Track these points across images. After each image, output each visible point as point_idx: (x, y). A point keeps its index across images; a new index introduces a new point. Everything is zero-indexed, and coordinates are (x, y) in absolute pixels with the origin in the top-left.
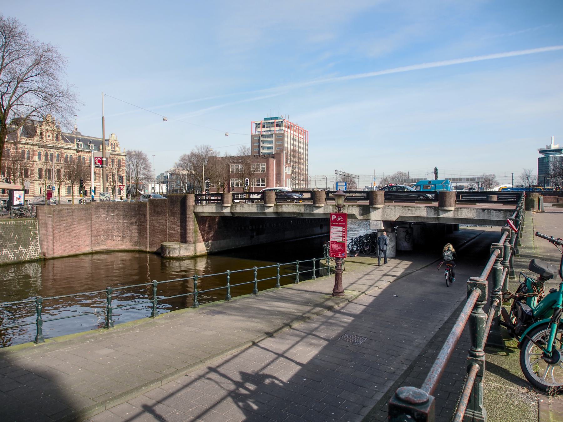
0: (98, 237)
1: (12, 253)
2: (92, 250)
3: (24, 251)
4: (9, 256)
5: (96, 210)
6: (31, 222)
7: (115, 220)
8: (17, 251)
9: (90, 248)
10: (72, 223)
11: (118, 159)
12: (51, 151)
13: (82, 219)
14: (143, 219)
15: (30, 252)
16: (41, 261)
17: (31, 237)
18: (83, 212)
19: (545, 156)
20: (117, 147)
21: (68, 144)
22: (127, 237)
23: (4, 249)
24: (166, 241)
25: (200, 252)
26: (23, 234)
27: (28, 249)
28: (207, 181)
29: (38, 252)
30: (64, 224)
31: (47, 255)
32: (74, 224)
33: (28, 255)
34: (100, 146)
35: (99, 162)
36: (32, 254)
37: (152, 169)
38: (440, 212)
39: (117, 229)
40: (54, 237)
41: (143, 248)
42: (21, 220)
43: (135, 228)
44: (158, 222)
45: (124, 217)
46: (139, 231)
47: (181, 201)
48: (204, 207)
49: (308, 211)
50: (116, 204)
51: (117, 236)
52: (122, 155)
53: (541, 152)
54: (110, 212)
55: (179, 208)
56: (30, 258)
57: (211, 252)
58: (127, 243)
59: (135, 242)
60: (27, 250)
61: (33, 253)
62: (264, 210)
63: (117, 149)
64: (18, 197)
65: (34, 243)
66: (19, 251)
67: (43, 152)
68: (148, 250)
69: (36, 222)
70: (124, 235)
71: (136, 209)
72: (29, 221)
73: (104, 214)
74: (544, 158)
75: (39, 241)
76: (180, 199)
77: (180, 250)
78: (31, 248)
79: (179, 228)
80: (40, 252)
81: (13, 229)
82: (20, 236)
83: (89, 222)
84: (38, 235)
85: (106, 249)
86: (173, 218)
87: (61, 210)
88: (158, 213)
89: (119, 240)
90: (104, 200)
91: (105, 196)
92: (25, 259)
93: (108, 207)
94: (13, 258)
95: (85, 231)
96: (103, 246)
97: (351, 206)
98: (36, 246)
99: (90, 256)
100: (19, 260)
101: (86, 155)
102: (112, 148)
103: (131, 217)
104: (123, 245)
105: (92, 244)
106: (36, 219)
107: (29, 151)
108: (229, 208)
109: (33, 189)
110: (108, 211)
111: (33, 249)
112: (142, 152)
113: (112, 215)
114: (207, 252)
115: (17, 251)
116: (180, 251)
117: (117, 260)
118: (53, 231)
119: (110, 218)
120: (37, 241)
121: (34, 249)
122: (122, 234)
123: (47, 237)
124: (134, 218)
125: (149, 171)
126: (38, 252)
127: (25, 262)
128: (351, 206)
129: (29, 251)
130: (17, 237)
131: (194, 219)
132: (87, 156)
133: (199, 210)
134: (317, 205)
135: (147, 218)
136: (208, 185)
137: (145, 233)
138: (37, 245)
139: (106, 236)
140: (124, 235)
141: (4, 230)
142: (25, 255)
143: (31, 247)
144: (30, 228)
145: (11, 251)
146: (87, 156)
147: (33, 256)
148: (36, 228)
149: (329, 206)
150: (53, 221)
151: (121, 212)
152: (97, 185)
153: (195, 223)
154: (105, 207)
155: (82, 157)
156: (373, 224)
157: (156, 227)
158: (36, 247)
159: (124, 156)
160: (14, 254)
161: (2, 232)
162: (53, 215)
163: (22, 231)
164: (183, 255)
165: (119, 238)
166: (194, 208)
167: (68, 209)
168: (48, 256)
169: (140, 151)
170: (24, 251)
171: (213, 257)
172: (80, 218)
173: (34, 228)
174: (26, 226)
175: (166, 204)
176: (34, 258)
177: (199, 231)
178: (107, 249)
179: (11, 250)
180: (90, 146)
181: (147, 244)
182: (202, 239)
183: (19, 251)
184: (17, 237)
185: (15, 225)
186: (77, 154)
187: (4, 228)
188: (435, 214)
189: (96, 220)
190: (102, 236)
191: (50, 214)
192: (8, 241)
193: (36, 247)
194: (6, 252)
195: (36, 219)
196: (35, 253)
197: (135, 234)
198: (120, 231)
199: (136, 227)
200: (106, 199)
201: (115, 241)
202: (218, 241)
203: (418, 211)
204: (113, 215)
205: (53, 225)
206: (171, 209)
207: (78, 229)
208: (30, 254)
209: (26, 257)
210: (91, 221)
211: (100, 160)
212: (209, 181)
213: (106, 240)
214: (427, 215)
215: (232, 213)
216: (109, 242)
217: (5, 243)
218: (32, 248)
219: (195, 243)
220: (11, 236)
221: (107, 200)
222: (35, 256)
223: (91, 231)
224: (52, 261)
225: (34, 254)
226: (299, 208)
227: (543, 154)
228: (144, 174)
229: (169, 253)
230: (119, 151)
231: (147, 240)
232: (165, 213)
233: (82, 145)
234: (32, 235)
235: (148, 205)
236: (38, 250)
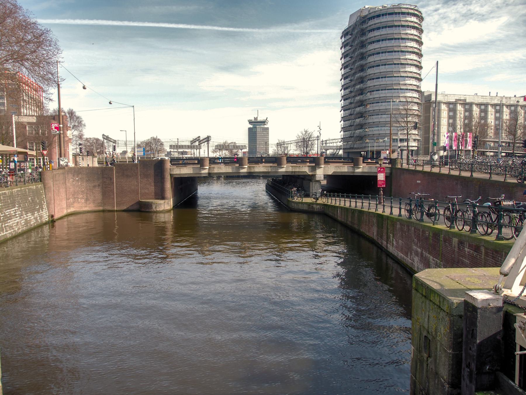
7: (79, 184)
19: (253, 126)
39: (81, 192)
41: (109, 208)
45: (87, 181)
46: (103, 192)
49: (274, 170)
50: (79, 169)
51: (82, 198)
53: (250, 122)
59: (99, 203)
62: (240, 171)
68: (115, 209)
89: (83, 202)
91: (65, 161)
103: (94, 181)
108: (208, 169)
110: (74, 176)
113: (77, 179)
122: (85, 196)
135: (114, 180)
140: (87, 197)
165: (83, 201)
166: (171, 170)
178: (75, 211)
198: (84, 193)
200: (65, 164)
211: (57, 126)
213: (74, 202)
226: (267, 168)
227: (252, 125)
229: (156, 208)
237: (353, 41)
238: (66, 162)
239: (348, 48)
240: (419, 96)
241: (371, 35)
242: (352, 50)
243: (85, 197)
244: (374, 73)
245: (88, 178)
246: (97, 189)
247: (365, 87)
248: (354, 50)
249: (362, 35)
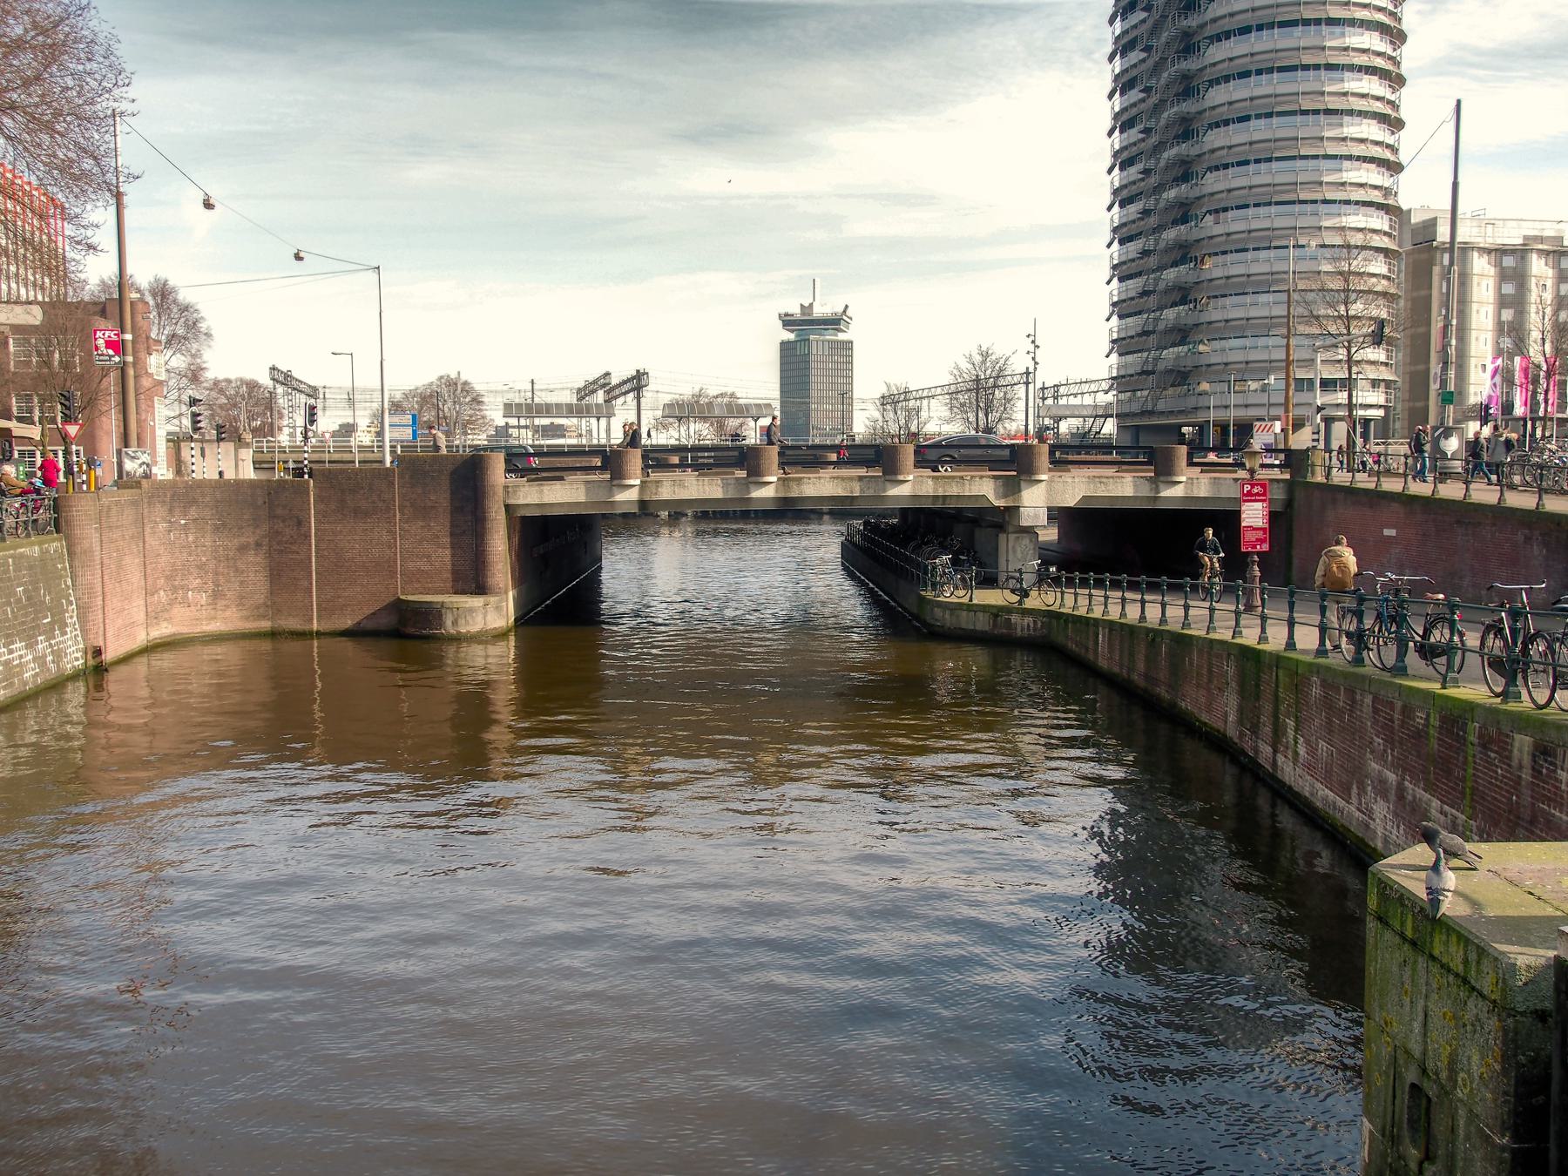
19: (797, 336)
22: (229, 594)
38: (1162, 486)
41: (293, 624)
44: (357, 538)
45: (217, 529)
49: (870, 493)
50: (191, 487)
51: (199, 590)
53: (788, 322)
54: (177, 511)
55: (448, 495)
58: (228, 613)
59: (258, 608)
68: (315, 627)
71: (260, 502)
74: (796, 342)
79: (448, 552)
93: (173, 496)
97: (977, 479)
99: (144, 659)
103: (241, 528)
105: (153, 617)
110: (171, 511)
113: (183, 522)
117: (197, 671)
124: (251, 529)
128: (977, 479)
134: (901, 478)
135: (310, 528)
140: (218, 586)
149: (925, 480)
151: (208, 513)
156: (1028, 516)
164: (492, 627)
165: (204, 598)
178: (174, 634)
188: (1151, 490)
197: (257, 582)
198: (206, 572)
201: (193, 608)
203: (1119, 485)
204: (185, 524)
211: (115, 338)
214: (1136, 492)
226: (848, 484)
227: (792, 331)
229: (455, 623)
231: (311, 597)
237: (1156, 29)
239: (1135, 56)
240: (1391, 227)
241: (1215, 139)
242: (1150, 63)
244: (1228, 187)
247: (1198, 195)
248: (1157, 63)
249: (1184, 8)
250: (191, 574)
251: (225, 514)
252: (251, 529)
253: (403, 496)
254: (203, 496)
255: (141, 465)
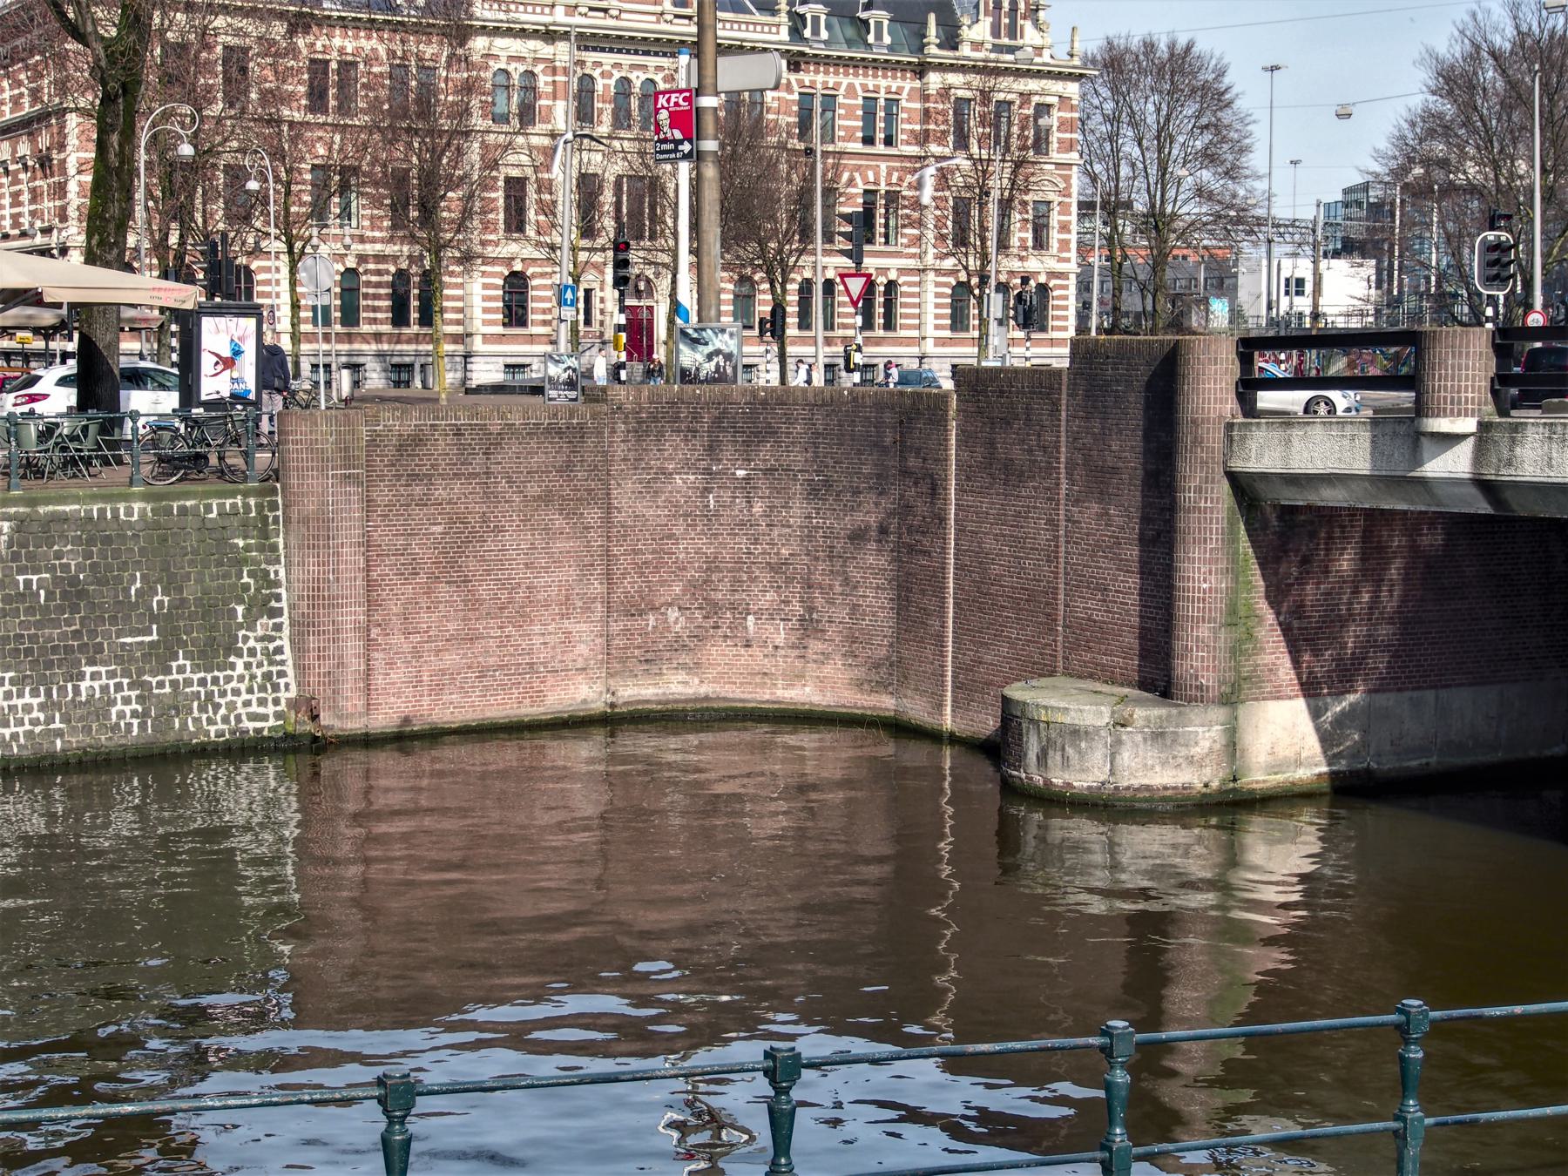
0: (651, 619)
1: (134, 694)
2: (610, 699)
3: (202, 682)
4: (114, 711)
5: (639, 439)
6: (247, 507)
7: (758, 508)
8: (161, 685)
9: (599, 686)
10: (484, 519)
11: (1035, 99)
12: (644, 67)
13: (546, 498)
14: (921, 507)
15: (236, 692)
16: (295, 750)
17: (240, 601)
18: (544, 455)
20: (1028, 25)
21: (741, 17)
23: (88, 670)
24: (1052, 674)
25: (1275, 768)
26: (199, 581)
27: (221, 675)
28: (1491, 236)
29: (283, 695)
30: (439, 529)
31: (326, 719)
32: (499, 530)
33: (223, 711)
34: (925, 24)
35: (677, 119)
36: (247, 704)
37: (1256, 160)
40: (371, 605)
41: (916, 710)
42: (186, 495)
43: (874, 561)
45: (813, 492)
47: (1149, 386)
48: (1297, 433)
50: (764, 403)
52: (1059, 76)
54: (728, 452)
56: (233, 732)
57: (1368, 771)
58: (828, 669)
59: (877, 666)
60: (215, 681)
61: (254, 698)
63: (1030, 35)
64: (227, 353)
65: (257, 640)
66: (174, 684)
67: (603, 74)
68: (948, 721)
69: (274, 507)
70: (811, 610)
71: (888, 441)
72: (234, 506)
73: (688, 466)
75: (286, 632)
76: (1143, 373)
77: (1118, 742)
78: (240, 669)
80: (293, 693)
81: (141, 550)
82: (180, 590)
83: (593, 515)
84: (282, 591)
85: (696, 700)
86: (1096, 507)
87: (417, 440)
88: (1008, 466)
89: (780, 639)
90: (703, 374)
92: (207, 733)
93: (717, 421)
94: (135, 722)
95: (569, 573)
96: (682, 676)
98: (272, 655)
99: (599, 736)
100: (171, 737)
101: (845, 82)
102: (996, 32)
103: (856, 492)
104: (800, 676)
106: (274, 491)
107: (530, 74)
108: (1466, 448)
109: (460, 299)
110: (712, 449)
111: (253, 677)
112: (1196, 50)
114: (1333, 775)
115: (161, 685)
116: (1113, 756)
118: (368, 569)
119: (726, 496)
120: (278, 627)
121: (259, 672)
123: (332, 603)
125: (1231, 173)
126: (283, 695)
127: (206, 752)
129: (228, 687)
130: (159, 598)
131: (1232, 524)
132: (851, 87)
133: (1260, 456)
136: (1496, 262)
137: (930, 603)
138: (279, 650)
139: (698, 615)
141: (88, 555)
142: (202, 709)
143: (240, 663)
144: (241, 543)
145: (126, 681)
146: (851, 87)
147: (253, 717)
148: (274, 548)
150: (369, 504)
152: (901, 271)
153: (1233, 557)
154: (696, 418)
155: (882, 102)
157: (995, 569)
158: (271, 663)
159: (1070, 77)
160: (140, 699)
161: (80, 568)
162: (369, 464)
163: (192, 563)
164: (1136, 783)
165: (780, 634)
166: (1230, 439)
167: (458, 433)
168: (337, 724)
169: (1182, 42)
170: (202, 682)
171: (1378, 819)
172: (533, 489)
173: (261, 549)
174: (217, 535)
175: (1055, 406)
176: (258, 731)
177: (1270, 617)
178: (707, 698)
179: (126, 673)
180: (866, 23)
181: (943, 683)
182: (1285, 671)
183: (174, 684)
184: (159, 598)
185: (157, 526)
186: (793, 77)
187: (91, 541)
189: (640, 508)
190: (673, 614)
191: (348, 461)
192: (114, 620)
193: (271, 663)
194: (96, 684)
195: (274, 491)
196: (263, 702)
197: (876, 602)
199: (883, 562)
200: (711, 366)
201: (755, 650)
202: (1429, 695)
204: (747, 479)
205: (367, 534)
206: (1088, 440)
207: (522, 559)
208: (231, 706)
209: (210, 721)
210: (609, 508)
211: (684, 105)
212: (1505, 236)
215: (1487, 488)
216: (718, 652)
217: (93, 633)
218: (248, 666)
219: (1232, 697)
220: (127, 590)
221: (719, 377)
222: (264, 718)
223: (609, 578)
224: (359, 755)
225: (255, 708)
228: (1201, 192)
229: (1042, 758)
230: (1039, 50)
231: (943, 655)
232: (1050, 469)
233: (823, 17)
234: (246, 587)
235: (952, 413)
236: (282, 681)
238: (569, 368)
243: (797, 607)
245: (818, 473)
246: (871, 560)
250: (753, 580)
251: (831, 462)
252: (873, 497)
253: (1074, 438)
254: (790, 422)
255: (565, 370)
